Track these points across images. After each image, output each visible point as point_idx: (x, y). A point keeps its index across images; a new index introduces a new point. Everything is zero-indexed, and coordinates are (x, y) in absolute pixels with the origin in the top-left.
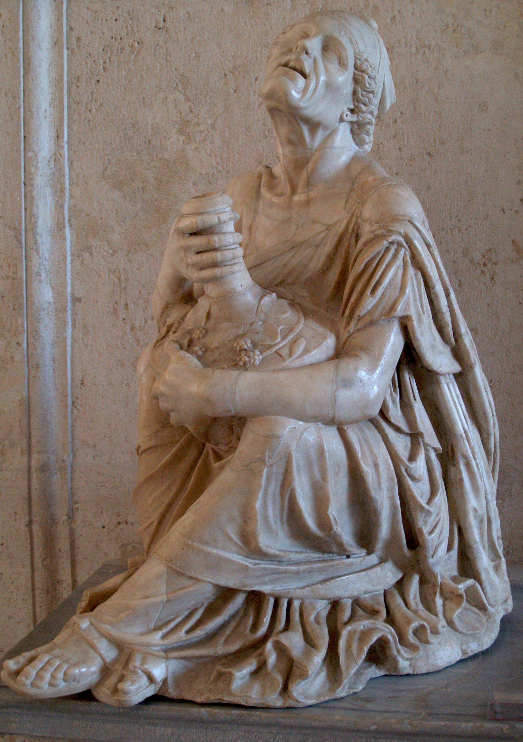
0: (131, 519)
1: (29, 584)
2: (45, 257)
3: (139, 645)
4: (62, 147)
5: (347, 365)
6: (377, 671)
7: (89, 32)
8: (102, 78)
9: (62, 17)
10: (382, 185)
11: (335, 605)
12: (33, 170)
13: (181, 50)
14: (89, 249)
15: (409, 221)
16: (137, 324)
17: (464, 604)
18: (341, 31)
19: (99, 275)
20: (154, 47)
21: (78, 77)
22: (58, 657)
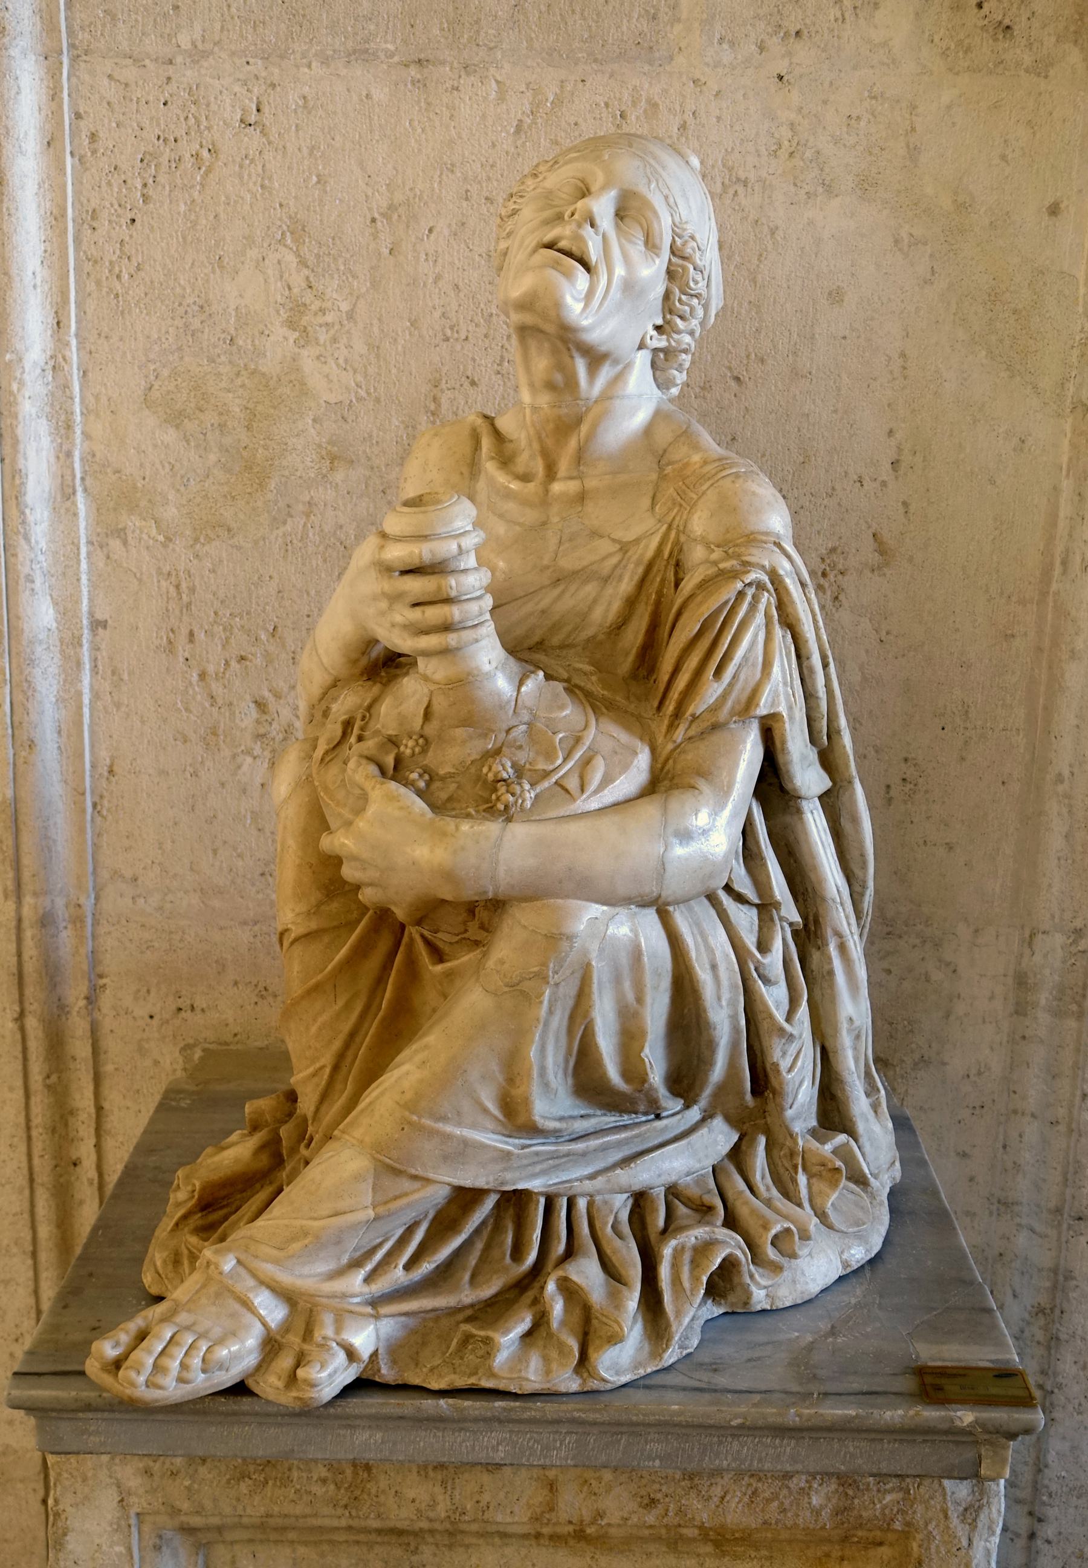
0: (200, 1002)
1: (22, 1119)
2: (40, 546)
3: (328, 1297)
4: (68, 344)
5: (678, 801)
6: (715, 1309)
7: (114, 125)
8: (139, 216)
9: (61, 91)
10: (724, 473)
11: (640, 1200)
12: (15, 387)
14: (120, 533)
15: (775, 543)
16: (211, 669)
17: (843, 1182)
19: (140, 580)
20: (238, 160)
21: (94, 210)
22: (188, 1328)
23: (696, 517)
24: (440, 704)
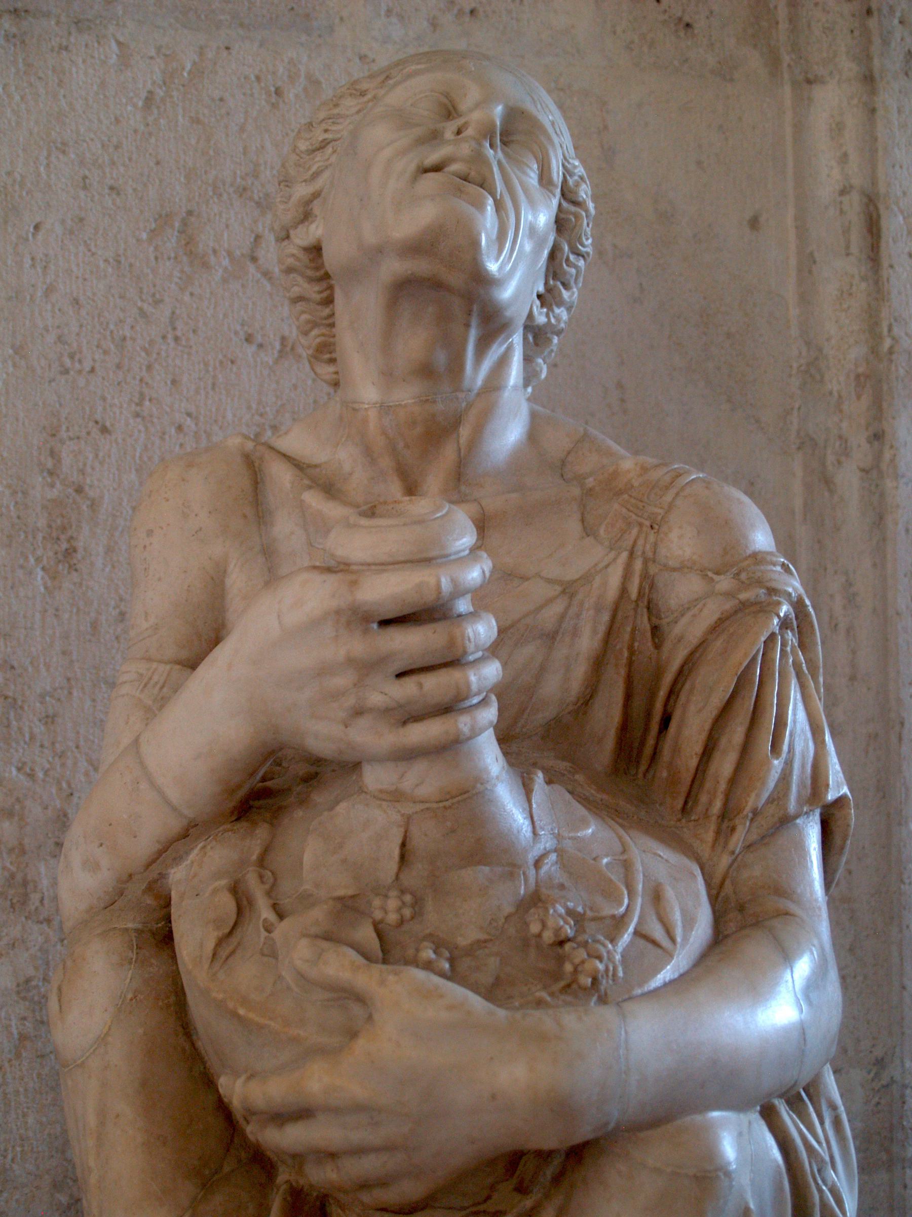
24: (427, 835)
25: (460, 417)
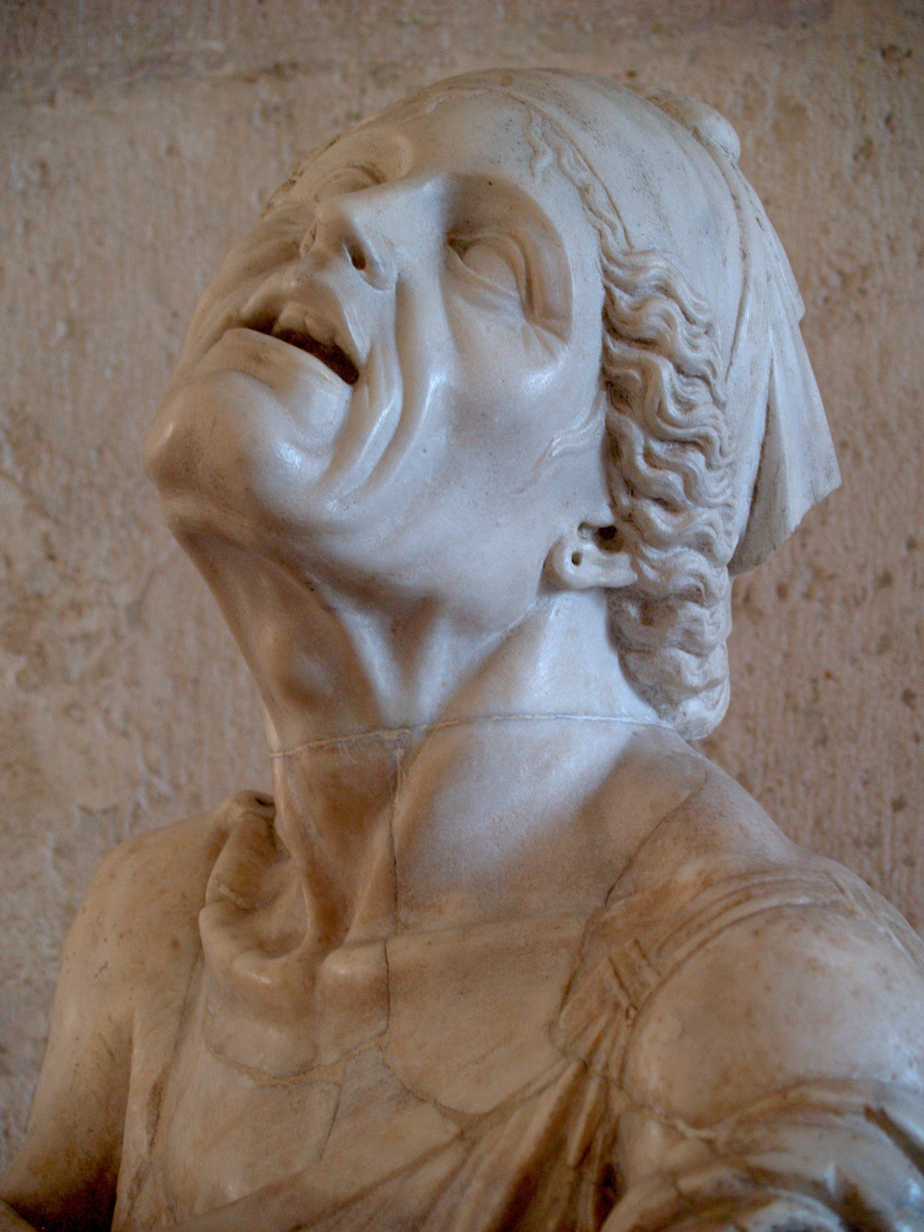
10: (737, 913)
13: (12, 311)
15: (869, 1113)
18: (535, 153)
23: (645, 1037)
25: (395, 777)
